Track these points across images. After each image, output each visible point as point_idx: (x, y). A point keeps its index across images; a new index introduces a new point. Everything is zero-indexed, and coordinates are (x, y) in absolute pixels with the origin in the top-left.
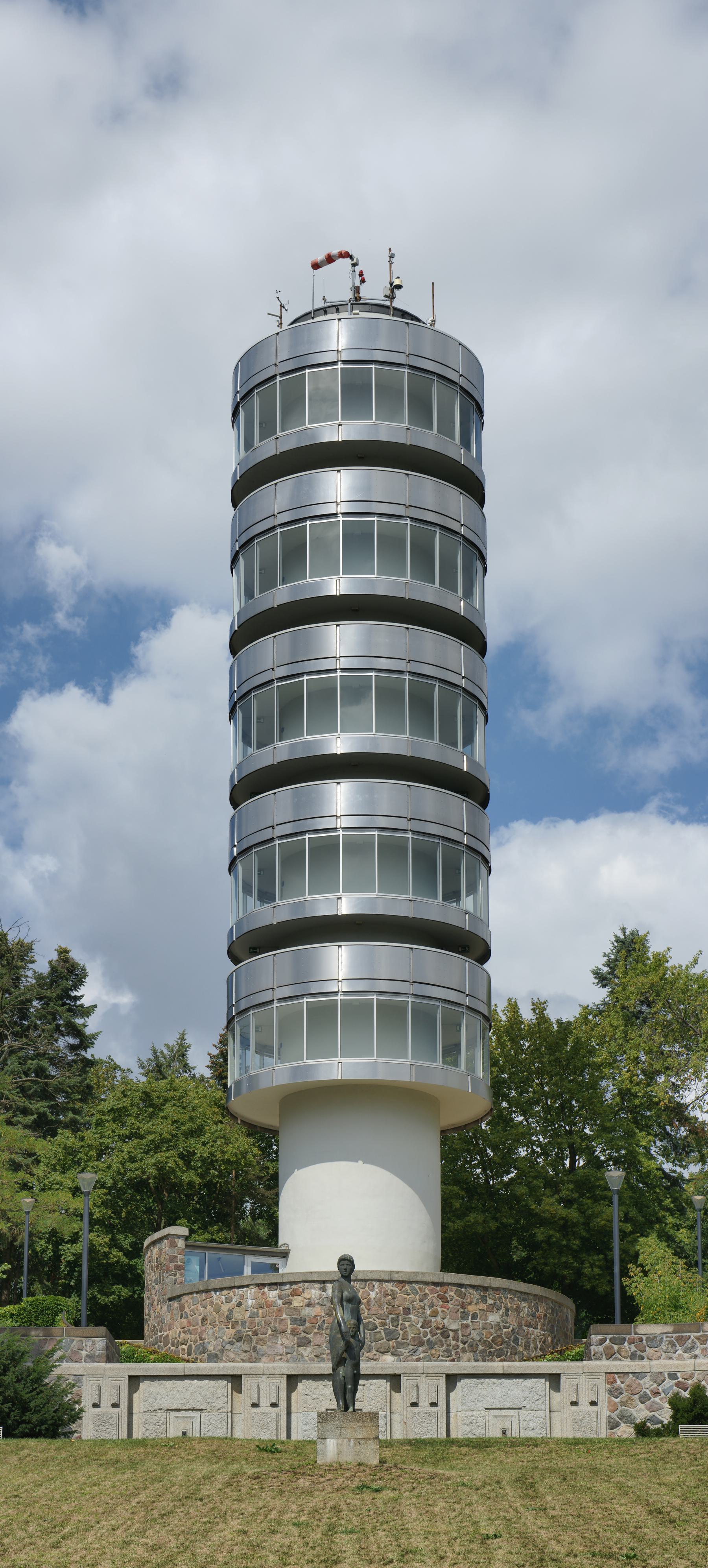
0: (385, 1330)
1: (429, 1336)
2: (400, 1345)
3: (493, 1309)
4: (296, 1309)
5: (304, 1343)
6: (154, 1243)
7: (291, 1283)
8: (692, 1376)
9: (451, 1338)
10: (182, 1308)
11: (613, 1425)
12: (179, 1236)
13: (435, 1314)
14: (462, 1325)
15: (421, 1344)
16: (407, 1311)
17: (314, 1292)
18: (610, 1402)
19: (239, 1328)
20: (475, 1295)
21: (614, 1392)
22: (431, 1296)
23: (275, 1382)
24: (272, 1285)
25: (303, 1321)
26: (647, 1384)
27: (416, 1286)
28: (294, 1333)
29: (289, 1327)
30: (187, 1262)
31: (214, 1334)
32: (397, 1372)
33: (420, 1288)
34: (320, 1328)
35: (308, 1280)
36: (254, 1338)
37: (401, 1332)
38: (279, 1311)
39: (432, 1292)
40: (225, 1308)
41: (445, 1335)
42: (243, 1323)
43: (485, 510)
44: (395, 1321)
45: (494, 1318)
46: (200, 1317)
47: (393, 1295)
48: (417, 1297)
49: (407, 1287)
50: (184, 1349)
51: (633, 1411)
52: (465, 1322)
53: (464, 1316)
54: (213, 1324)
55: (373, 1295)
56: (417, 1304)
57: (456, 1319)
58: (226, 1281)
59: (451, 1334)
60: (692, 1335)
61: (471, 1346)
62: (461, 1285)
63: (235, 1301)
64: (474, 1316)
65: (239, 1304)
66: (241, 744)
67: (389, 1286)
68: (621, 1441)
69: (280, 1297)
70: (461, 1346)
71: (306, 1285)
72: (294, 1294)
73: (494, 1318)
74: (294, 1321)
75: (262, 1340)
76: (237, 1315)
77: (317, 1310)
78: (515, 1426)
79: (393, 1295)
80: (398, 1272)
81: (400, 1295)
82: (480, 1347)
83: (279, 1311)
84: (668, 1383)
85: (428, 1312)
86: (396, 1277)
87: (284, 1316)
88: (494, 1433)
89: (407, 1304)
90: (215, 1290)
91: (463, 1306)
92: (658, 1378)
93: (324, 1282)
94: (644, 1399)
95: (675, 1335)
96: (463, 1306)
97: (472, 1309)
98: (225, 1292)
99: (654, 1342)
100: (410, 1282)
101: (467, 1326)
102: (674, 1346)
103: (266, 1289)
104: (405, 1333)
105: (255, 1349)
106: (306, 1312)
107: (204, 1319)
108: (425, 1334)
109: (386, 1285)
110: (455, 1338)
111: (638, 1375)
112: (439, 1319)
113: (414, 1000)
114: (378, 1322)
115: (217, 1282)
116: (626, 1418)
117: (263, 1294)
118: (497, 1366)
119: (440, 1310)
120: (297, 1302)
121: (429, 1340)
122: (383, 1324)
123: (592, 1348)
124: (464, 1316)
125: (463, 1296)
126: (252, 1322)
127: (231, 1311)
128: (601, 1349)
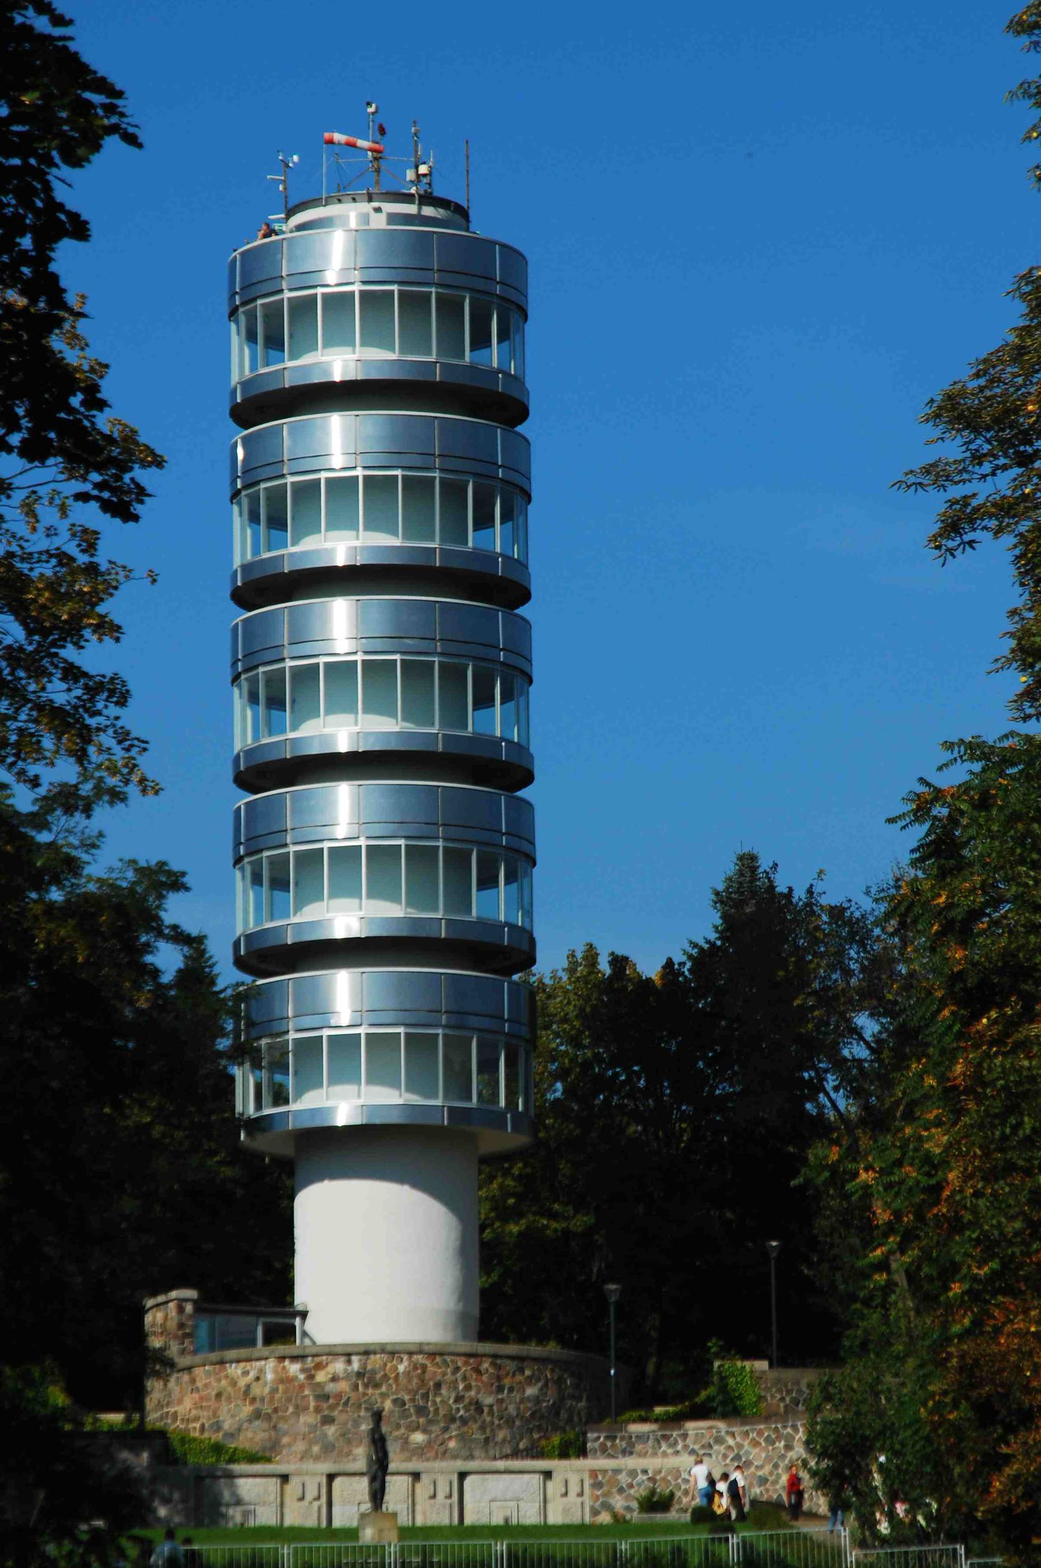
0: (415, 1406)
1: (462, 1412)
2: (430, 1422)
3: (530, 1380)
4: (318, 1384)
5: (328, 1420)
6: (157, 1305)
7: (314, 1356)
8: (660, 1472)
9: (485, 1414)
10: (193, 1381)
11: (595, 1513)
12: (186, 1300)
13: (468, 1388)
14: (498, 1400)
15: (453, 1420)
16: (438, 1386)
17: (338, 1366)
18: (592, 1495)
19: (258, 1405)
20: (511, 1366)
21: (597, 1485)
22: (464, 1369)
23: (318, 1479)
24: (294, 1358)
25: (326, 1397)
26: (623, 1479)
27: (448, 1359)
28: (318, 1410)
29: (312, 1404)
30: (195, 1327)
31: (229, 1411)
32: (417, 1471)
33: (452, 1361)
34: (346, 1404)
35: (333, 1352)
36: (274, 1417)
37: (431, 1409)
38: (302, 1387)
39: (466, 1363)
40: (242, 1382)
41: (479, 1407)
42: (263, 1400)
43: (530, 507)
44: (425, 1396)
45: (531, 1391)
46: (214, 1393)
47: (424, 1367)
48: (449, 1370)
49: (438, 1359)
50: (195, 1428)
51: (612, 1501)
52: (500, 1397)
53: (500, 1389)
54: (229, 1399)
55: (401, 1368)
56: (449, 1377)
57: (491, 1393)
58: (243, 1352)
59: (486, 1410)
60: (675, 1434)
61: (507, 1422)
62: (495, 1356)
63: (252, 1375)
64: (511, 1389)
65: (258, 1379)
66: (362, 1349)
67: (419, 1358)
68: (601, 1527)
69: (303, 1370)
70: (496, 1422)
71: (330, 1358)
72: (319, 1366)
73: (531, 1391)
74: (318, 1397)
75: (283, 1417)
76: (256, 1390)
77: (343, 1386)
78: (515, 1515)
79: (424, 1367)
80: (428, 1344)
81: (431, 1368)
82: (518, 1423)
83: (302, 1387)
84: (641, 1477)
85: (461, 1387)
86: (426, 1348)
87: (306, 1392)
88: (497, 1520)
89: (438, 1378)
90: (231, 1362)
91: (499, 1378)
92: (633, 1473)
93: (349, 1355)
94: (621, 1490)
95: (660, 1433)
96: (499, 1378)
97: (507, 1382)
98: (242, 1364)
99: (642, 1438)
100: (441, 1354)
101: (502, 1401)
102: (659, 1443)
103: (287, 1363)
104: (437, 1410)
105: (275, 1427)
106: (331, 1387)
107: (219, 1395)
108: (458, 1410)
109: (415, 1357)
110: (491, 1412)
111: (617, 1471)
112: (473, 1393)
113: (448, 1031)
114: (407, 1398)
115: (232, 1354)
116: (607, 1507)
117: (284, 1368)
118: (501, 1464)
119: (473, 1384)
120: (321, 1377)
121: (461, 1416)
122: (413, 1400)
123: (589, 1445)
124: (500, 1389)
125: (499, 1368)
126: (272, 1399)
127: (248, 1387)
128: (596, 1445)
